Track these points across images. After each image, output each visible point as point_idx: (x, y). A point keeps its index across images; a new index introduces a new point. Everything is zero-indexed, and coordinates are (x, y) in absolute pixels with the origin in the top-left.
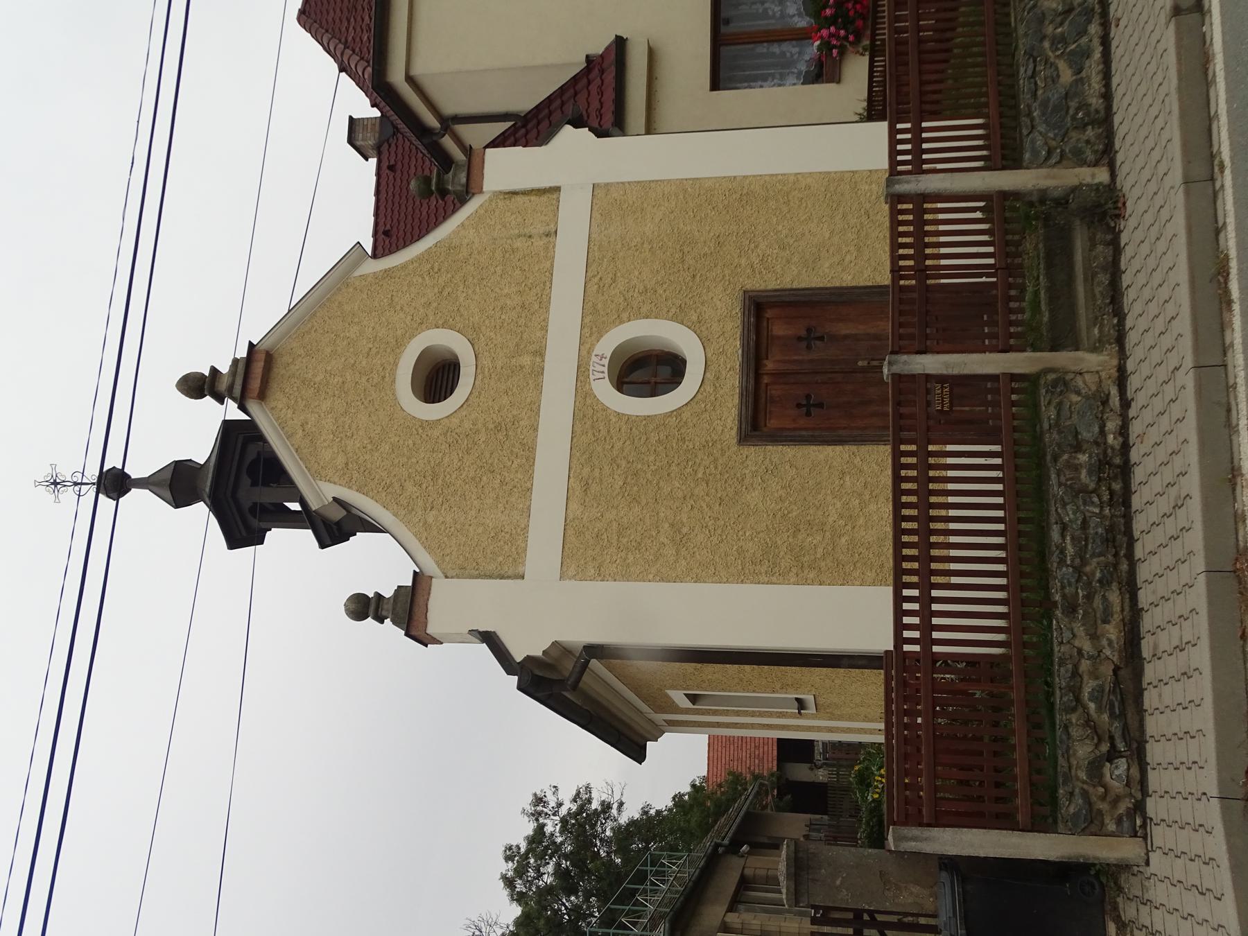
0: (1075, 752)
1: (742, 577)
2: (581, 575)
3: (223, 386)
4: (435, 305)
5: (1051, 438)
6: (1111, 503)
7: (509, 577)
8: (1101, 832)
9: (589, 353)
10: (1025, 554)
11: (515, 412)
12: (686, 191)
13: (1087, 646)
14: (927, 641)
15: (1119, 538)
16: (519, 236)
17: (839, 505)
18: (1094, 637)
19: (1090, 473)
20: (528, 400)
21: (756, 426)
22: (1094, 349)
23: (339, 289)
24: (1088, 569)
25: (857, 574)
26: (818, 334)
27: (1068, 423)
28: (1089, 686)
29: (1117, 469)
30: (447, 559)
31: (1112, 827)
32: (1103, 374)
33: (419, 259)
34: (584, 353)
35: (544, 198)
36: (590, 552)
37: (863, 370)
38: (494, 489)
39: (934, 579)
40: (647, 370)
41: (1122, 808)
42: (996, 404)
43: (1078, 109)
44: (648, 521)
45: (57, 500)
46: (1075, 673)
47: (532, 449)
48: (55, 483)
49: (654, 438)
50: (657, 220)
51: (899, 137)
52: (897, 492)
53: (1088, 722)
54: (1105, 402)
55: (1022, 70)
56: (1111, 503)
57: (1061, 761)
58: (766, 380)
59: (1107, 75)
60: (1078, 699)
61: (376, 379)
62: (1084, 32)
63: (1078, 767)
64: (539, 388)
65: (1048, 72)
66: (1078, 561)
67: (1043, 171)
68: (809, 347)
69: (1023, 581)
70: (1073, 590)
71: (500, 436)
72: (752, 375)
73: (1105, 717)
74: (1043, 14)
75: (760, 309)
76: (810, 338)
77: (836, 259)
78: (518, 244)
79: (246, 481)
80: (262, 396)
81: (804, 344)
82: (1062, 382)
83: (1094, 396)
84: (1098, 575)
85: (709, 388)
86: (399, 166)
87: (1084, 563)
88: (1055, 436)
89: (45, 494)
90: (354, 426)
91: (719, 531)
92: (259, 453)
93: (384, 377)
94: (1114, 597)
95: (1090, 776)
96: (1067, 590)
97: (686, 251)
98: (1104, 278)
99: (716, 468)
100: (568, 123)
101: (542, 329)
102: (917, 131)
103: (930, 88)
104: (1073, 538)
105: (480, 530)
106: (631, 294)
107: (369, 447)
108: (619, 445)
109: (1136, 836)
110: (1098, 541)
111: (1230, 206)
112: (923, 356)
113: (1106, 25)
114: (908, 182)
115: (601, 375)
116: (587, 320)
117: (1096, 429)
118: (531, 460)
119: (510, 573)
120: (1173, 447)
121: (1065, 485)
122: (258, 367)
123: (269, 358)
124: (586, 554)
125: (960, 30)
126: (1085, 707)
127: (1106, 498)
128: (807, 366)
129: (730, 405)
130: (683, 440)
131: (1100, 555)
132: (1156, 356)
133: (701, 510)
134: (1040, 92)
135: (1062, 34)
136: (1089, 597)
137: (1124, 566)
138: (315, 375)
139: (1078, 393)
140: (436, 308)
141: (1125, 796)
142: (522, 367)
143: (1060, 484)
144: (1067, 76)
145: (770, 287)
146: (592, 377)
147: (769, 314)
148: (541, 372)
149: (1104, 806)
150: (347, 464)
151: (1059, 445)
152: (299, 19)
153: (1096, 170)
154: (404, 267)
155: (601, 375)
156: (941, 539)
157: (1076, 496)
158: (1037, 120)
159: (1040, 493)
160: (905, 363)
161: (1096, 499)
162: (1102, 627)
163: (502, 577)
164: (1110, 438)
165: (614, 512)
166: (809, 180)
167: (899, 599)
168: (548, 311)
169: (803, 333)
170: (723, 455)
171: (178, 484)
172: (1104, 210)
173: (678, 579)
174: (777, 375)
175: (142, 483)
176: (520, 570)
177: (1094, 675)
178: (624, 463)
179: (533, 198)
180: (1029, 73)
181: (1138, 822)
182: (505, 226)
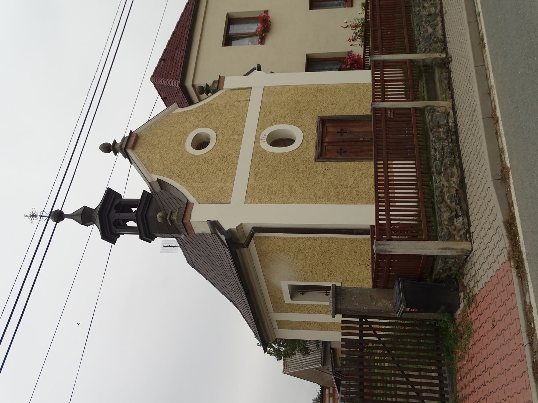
0: (443, 216)
1: (316, 202)
2: (253, 202)
3: (117, 147)
6: (452, 142)
8: (454, 240)
9: (260, 134)
13: (446, 184)
14: (389, 220)
15: (456, 152)
17: (353, 180)
18: (448, 181)
19: (444, 134)
22: (443, 100)
24: (445, 162)
29: (454, 133)
31: (458, 238)
33: (198, 108)
36: (257, 195)
37: (362, 141)
41: (462, 232)
43: (434, 38)
44: (280, 185)
46: (442, 191)
49: (283, 160)
52: (376, 176)
54: (448, 114)
56: (452, 142)
59: (443, 25)
60: (443, 199)
62: (436, 19)
65: (424, 29)
66: (441, 159)
67: (424, 54)
68: (341, 135)
71: (224, 159)
72: (320, 141)
73: (454, 204)
76: (341, 132)
77: (352, 108)
78: (235, 103)
79: (114, 211)
80: (133, 148)
82: (433, 110)
83: (444, 113)
87: (443, 159)
89: (28, 220)
94: (455, 170)
95: (449, 222)
96: (438, 168)
98: (446, 82)
103: (384, 34)
104: (439, 152)
109: (467, 241)
117: (445, 121)
122: (133, 139)
123: (137, 137)
124: (254, 195)
126: (446, 202)
127: (450, 141)
131: (449, 157)
136: (446, 169)
137: (458, 161)
139: (439, 112)
141: (462, 229)
143: (433, 137)
144: (430, 30)
147: (327, 125)
149: (455, 232)
151: (432, 126)
152: (151, 79)
156: (394, 204)
157: (440, 140)
162: (450, 179)
164: (451, 124)
167: (377, 211)
168: (245, 122)
171: (85, 216)
172: (445, 64)
175: (69, 216)
176: (229, 201)
177: (449, 192)
181: (468, 235)
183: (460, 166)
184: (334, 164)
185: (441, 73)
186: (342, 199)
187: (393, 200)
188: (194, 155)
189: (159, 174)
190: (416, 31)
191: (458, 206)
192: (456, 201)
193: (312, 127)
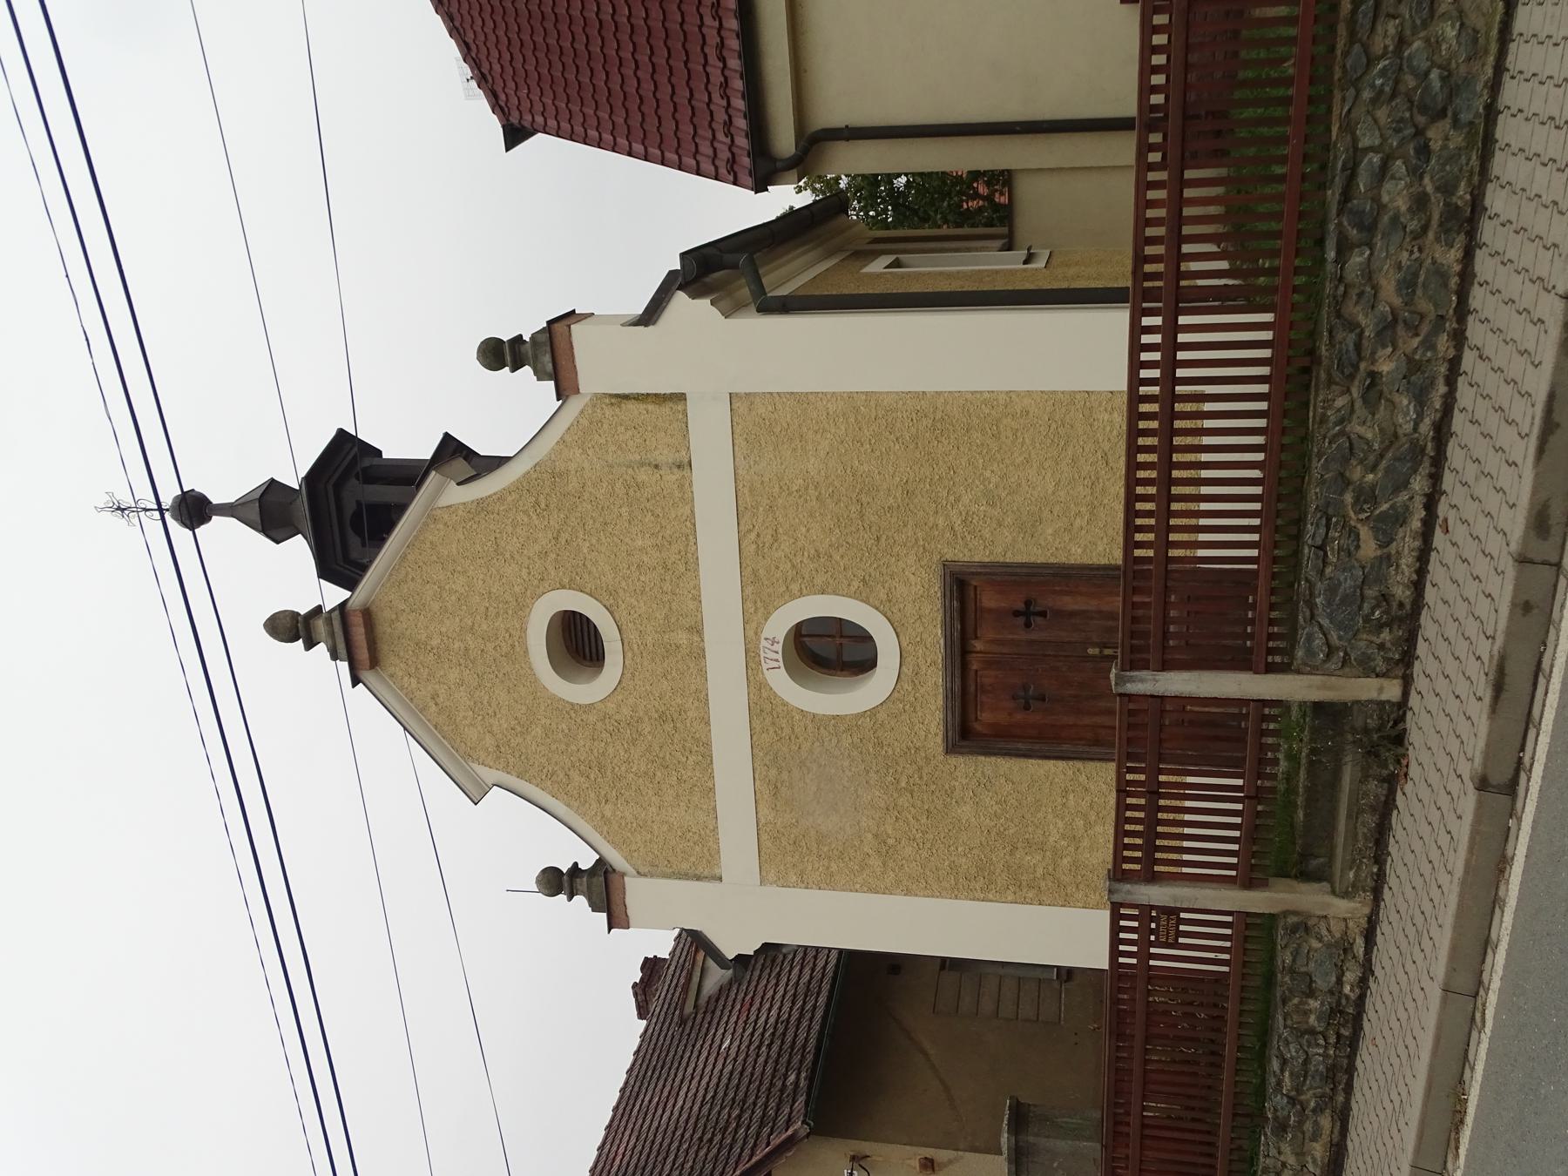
16: (642, 464)
17: (1060, 824)
18: (1300, 1154)
19: (1319, 1019)
20: (693, 687)
21: (967, 733)
22: (1345, 895)
25: (1080, 895)
26: (1038, 609)
27: (1303, 969)
29: (1347, 1022)
32: (1351, 924)
34: (751, 633)
35: (666, 409)
40: (829, 651)
47: (708, 745)
50: (822, 454)
51: (1139, 522)
64: (702, 673)
68: (1028, 625)
71: (669, 727)
72: (958, 673)
75: (962, 587)
76: (1027, 614)
78: (643, 475)
79: (354, 540)
80: (374, 663)
81: (1021, 620)
82: (1303, 926)
84: (1312, 1104)
88: (1287, 979)
90: (494, 704)
92: (359, 503)
93: (513, 646)
94: (1325, 1122)
97: (864, 499)
98: (1370, 820)
101: (694, 598)
104: (1291, 1074)
105: (665, 828)
113: (1436, 478)
114: (1142, 681)
115: (775, 664)
116: (749, 590)
118: (708, 757)
119: (706, 873)
127: (1333, 1040)
128: (1025, 662)
130: (881, 744)
133: (906, 822)
134: (1328, 570)
135: (1373, 487)
137: (1341, 1098)
138: (430, 637)
139: (1320, 940)
144: (1369, 548)
146: (765, 667)
151: (1290, 990)
154: (500, 497)
155: (775, 664)
157: (1302, 1035)
160: (1129, 892)
161: (1322, 1042)
163: (698, 878)
164: (1347, 989)
169: (1020, 606)
171: (270, 511)
172: (1386, 737)
173: (887, 891)
175: (228, 510)
176: (717, 871)
179: (651, 407)
182: (620, 447)
183: (1343, 1117)
184: (1005, 765)
185: (1365, 778)
186: (1030, 887)
189: (489, 761)
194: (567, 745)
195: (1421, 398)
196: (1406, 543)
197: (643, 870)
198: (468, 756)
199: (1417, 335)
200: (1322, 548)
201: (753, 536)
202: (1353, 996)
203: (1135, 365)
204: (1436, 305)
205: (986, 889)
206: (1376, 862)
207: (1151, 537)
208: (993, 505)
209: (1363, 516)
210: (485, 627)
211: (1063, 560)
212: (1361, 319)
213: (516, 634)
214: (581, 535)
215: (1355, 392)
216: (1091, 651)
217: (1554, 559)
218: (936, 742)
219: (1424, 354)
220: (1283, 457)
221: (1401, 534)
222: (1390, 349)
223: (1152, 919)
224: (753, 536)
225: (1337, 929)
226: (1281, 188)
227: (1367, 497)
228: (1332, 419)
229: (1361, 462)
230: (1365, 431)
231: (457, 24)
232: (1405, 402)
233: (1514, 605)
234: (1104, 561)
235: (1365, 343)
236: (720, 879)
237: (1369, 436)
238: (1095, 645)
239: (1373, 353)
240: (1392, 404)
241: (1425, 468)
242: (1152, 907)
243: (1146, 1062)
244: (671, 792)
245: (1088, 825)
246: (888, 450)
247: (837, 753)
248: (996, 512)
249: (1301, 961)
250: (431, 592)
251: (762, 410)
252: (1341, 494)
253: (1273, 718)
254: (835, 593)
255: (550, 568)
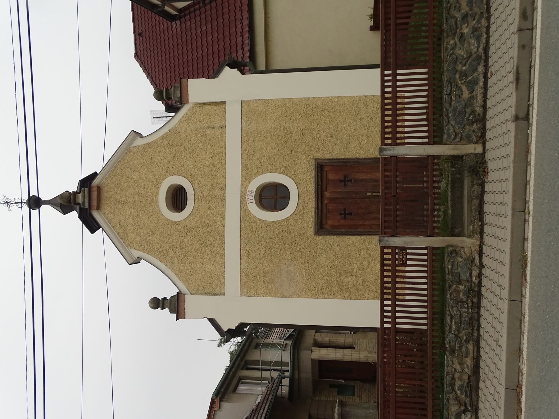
1: (317, 295)
4: (172, 163)
5: (449, 277)
6: (472, 307)
7: (218, 294)
9: (245, 189)
10: (436, 298)
11: (214, 218)
12: (286, 105)
13: (458, 367)
14: (394, 323)
15: (474, 322)
16: (208, 127)
17: (358, 263)
18: (461, 364)
19: (464, 294)
21: (321, 228)
22: (470, 236)
23: (126, 153)
24: (460, 335)
25: (366, 294)
27: (456, 271)
28: (457, 384)
29: (475, 293)
30: (191, 285)
32: (473, 249)
34: (243, 189)
35: (219, 107)
37: (369, 197)
38: (208, 254)
39: (397, 297)
42: (427, 216)
43: (470, 114)
45: (10, 210)
46: (453, 378)
47: (223, 236)
48: (7, 203)
50: (273, 121)
53: (457, 399)
54: (472, 262)
55: (445, 89)
56: (472, 307)
57: (445, 412)
58: (326, 202)
60: (453, 389)
61: (150, 200)
62: (476, 70)
63: (452, 415)
64: (224, 206)
65: (457, 92)
66: (457, 332)
67: (452, 146)
68: (345, 185)
69: (433, 286)
70: (454, 343)
71: (209, 229)
72: (319, 202)
73: (464, 396)
74: (457, 58)
75: (321, 167)
76: (345, 181)
78: (208, 131)
81: (343, 184)
82: (455, 252)
83: (468, 259)
84: (465, 338)
85: (301, 208)
86: (144, 34)
87: (459, 332)
88: (450, 276)
90: (142, 223)
91: (307, 275)
93: (153, 199)
94: (471, 347)
97: (287, 137)
98: (476, 202)
99: (305, 246)
100: (227, 65)
101: (223, 177)
102: (395, 75)
104: (455, 322)
105: (204, 273)
106: (263, 160)
107: (151, 233)
108: (261, 235)
110: (466, 323)
111: (539, 18)
112: (395, 238)
114: (389, 150)
116: (243, 173)
117: (468, 275)
118: (223, 241)
119: (218, 292)
120: (504, 51)
121: (453, 299)
124: (252, 284)
125: (416, 11)
126: (456, 392)
127: (470, 305)
129: (310, 216)
132: (503, 16)
134: (453, 103)
135: (465, 71)
136: (460, 347)
138: (121, 197)
139: (462, 257)
140: (173, 165)
142: (215, 196)
143: (451, 299)
144: (466, 94)
145: (327, 157)
147: (326, 169)
148: (224, 199)
150: (141, 241)
151: (452, 281)
153: (477, 146)
155: (252, 201)
156: (402, 280)
157: (458, 304)
158: (451, 117)
159: (443, 303)
161: (466, 306)
163: (215, 295)
165: (261, 266)
166: (344, 100)
167: (382, 305)
168: (225, 168)
169: (342, 178)
170: (308, 240)
171: (65, 203)
172: (478, 168)
174: (332, 200)
175: (48, 202)
176: (223, 291)
177: (460, 379)
178: (264, 244)
179: (213, 107)
180: (448, 92)
182: (201, 122)
186: (347, 292)
187: (403, 135)
188: (173, 221)
190: (446, 90)
191: (468, 399)
192: (466, 392)
193: (308, 177)
194: (169, 239)
195: (478, 39)
196: (479, 91)
197: (193, 292)
198: (129, 246)
199: (474, 20)
200: (450, 94)
201: (247, 151)
202: (476, 282)
203: (383, 87)
204: (480, 9)
205: (329, 294)
206: (480, 221)
207: (390, 89)
208: (333, 137)
209: (463, 82)
210: (143, 192)
211: (358, 157)
212: (456, 15)
213: (154, 194)
214: (183, 155)
215: (456, 39)
216: (369, 194)
217: (530, 27)
218: (311, 230)
219: (477, 25)
220: (434, 82)
221: (476, 88)
222: (466, 25)
223: (397, 254)
224: (247, 151)
225: (467, 251)
226: (427, 46)
227: (464, 75)
228: (449, 48)
229: (461, 63)
230: (461, 52)
231: (154, 79)
232: (473, 41)
233: (519, 46)
234: (372, 157)
235: (458, 22)
236: (224, 295)
237: (463, 54)
238: (370, 192)
239: (461, 26)
240: (469, 43)
241: (482, 63)
242: (397, 248)
243: (396, 396)
244: (207, 257)
245: (369, 264)
246: (296, 119)
247: (273, 237)
248: (334, 140)
249: (455, 267)
250: (124, 179)
251: (252, 106)
252: (455, 74)
253: (437, 164)
254: (275, 172)
255: (171, 168)
